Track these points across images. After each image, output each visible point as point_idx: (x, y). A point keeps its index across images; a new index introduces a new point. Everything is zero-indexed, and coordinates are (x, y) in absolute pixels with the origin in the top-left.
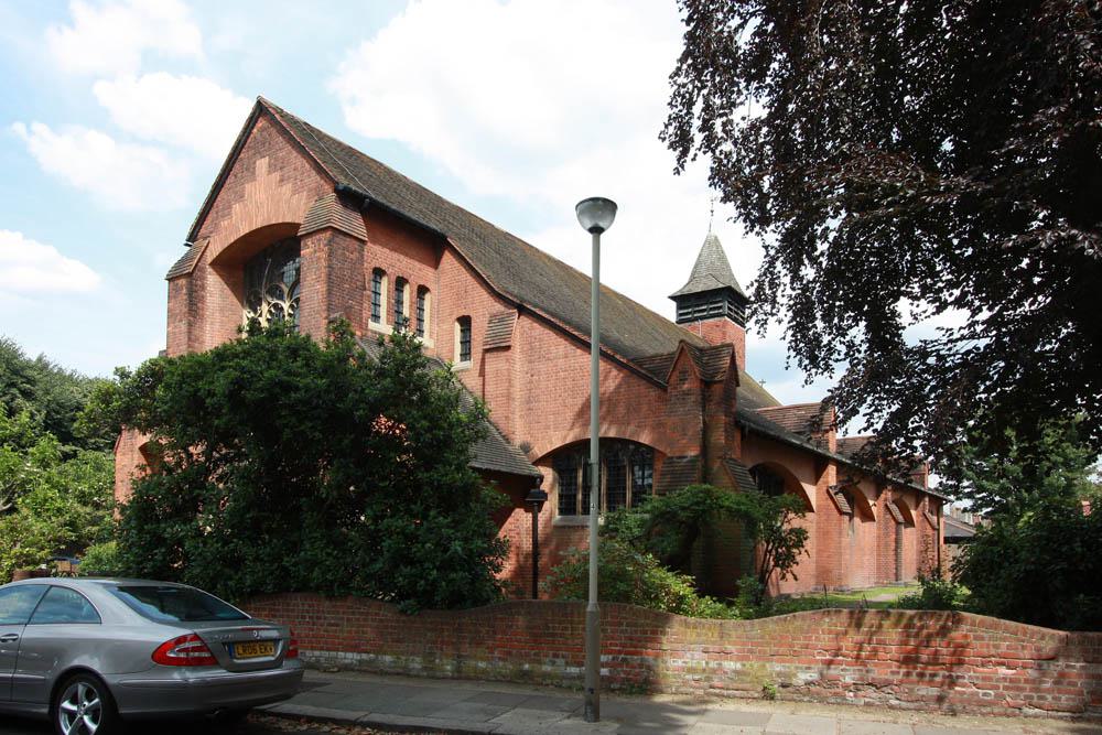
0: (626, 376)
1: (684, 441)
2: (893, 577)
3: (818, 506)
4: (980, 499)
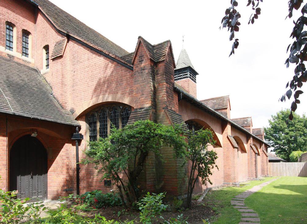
0: (116, 66)
1: (142, 99)
2: (255, 176)
4: (276, 147)
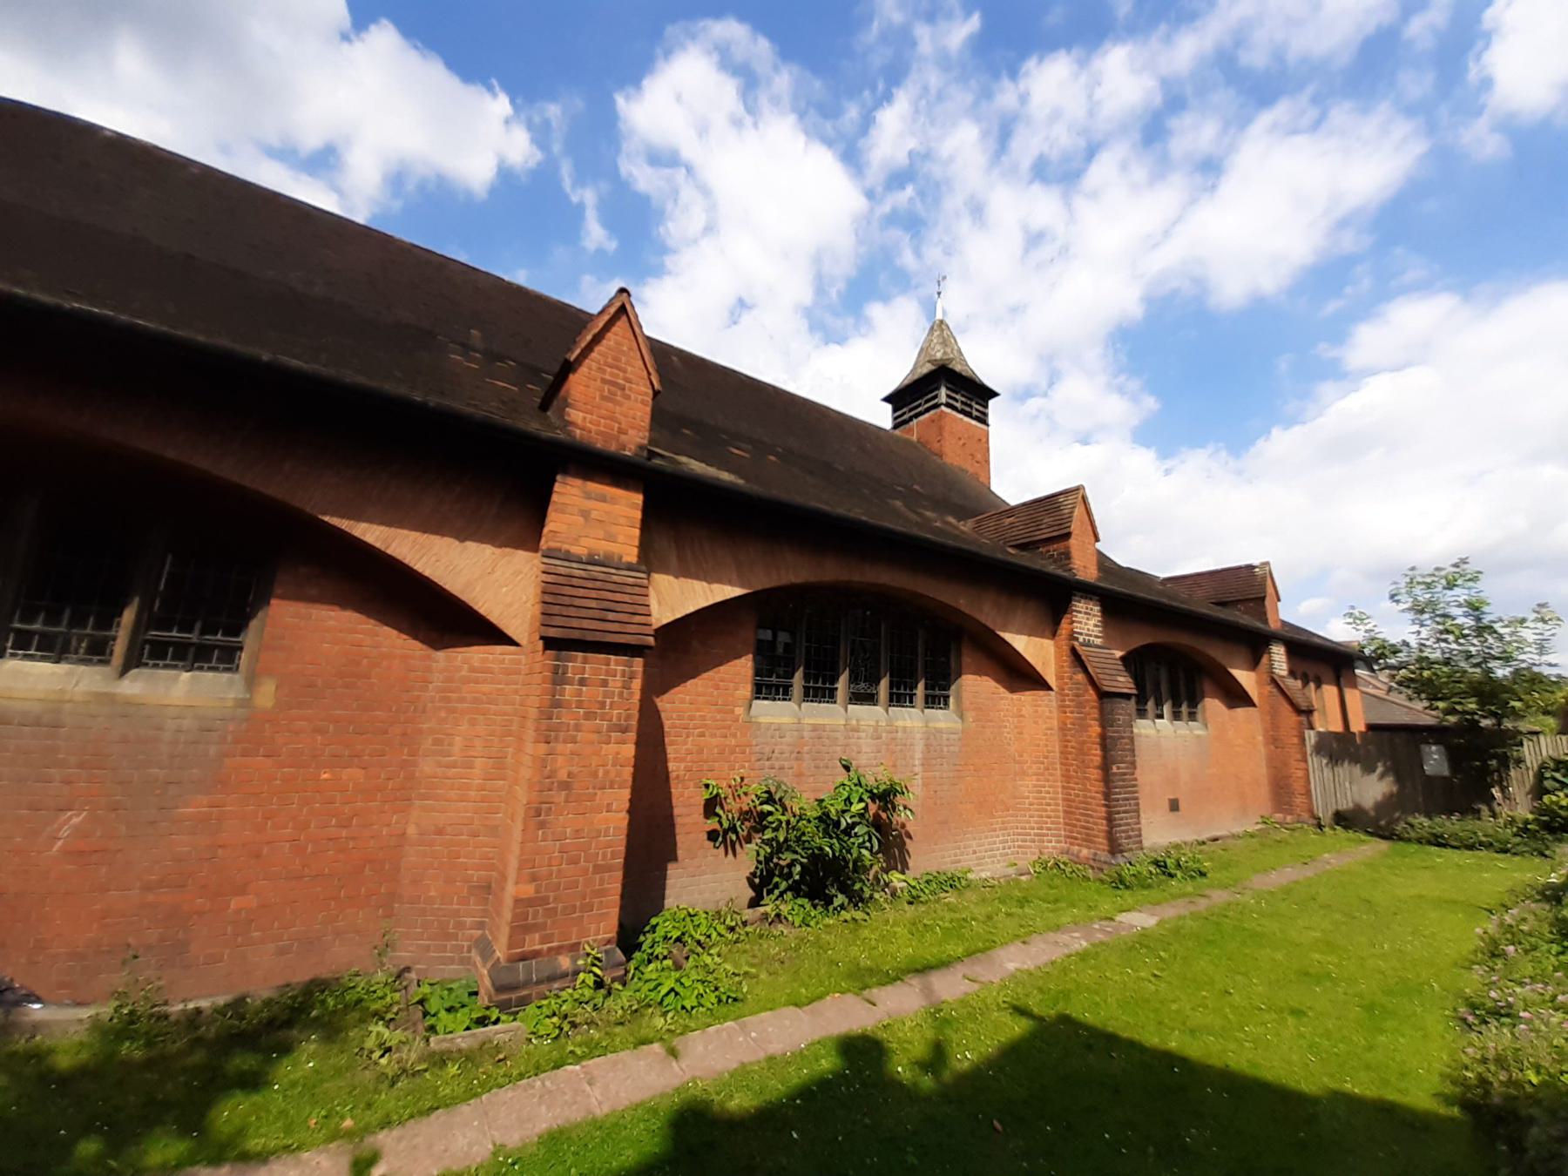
3: (1260, 694)
